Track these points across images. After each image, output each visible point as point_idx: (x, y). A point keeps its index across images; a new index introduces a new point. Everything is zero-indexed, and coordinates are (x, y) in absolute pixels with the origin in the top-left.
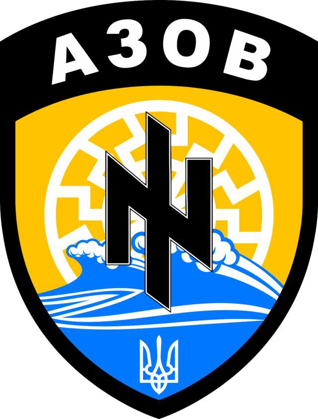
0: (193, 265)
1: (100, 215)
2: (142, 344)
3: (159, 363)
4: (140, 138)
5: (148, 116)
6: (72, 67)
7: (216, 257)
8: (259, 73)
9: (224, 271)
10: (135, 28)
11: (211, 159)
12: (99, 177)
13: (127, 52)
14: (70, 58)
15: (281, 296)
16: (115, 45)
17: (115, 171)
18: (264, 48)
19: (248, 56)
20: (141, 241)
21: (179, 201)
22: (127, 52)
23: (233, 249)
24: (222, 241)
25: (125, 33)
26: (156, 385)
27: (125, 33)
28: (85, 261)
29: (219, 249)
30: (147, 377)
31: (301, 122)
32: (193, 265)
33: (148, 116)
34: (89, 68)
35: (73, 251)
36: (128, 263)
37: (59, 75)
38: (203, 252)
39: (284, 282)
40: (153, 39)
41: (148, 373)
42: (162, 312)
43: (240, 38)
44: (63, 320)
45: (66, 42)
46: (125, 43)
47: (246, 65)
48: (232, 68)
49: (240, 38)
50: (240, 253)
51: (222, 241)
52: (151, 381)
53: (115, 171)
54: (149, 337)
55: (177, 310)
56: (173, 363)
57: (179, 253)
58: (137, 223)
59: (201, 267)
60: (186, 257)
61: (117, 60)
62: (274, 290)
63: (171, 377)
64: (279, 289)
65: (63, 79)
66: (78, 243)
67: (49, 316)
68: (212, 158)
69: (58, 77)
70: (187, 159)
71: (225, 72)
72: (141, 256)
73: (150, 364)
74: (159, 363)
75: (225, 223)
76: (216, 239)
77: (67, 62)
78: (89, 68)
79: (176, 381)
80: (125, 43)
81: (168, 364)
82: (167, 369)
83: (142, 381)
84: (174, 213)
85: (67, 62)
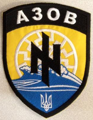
0: (55, 74)
1: (29, 59)
2: (42, 96)
3: (46, 101)
4: (41, 39)
6: (22, 20)
7: (62, 72)
8: (74, 22)
9: (64, 76)
10: (39, 10)
12: (29, 49)
13: (37, 16)
14: (22, 17)
15: (82, 84)
16: (34, 14)
17: (33, 47)
18: (75, 15)
19: (71, 18)
20: (41, 67)
21: (51, 55)
22: (37, 16)
23: (66, 70)
25: (37, 11)
26: (46, 109)
27: (37, 11)
28: (24, 71)
29: (63, 70)
30: (43, 106)
32: (55, 74)
34: (27, 20)
35: (22, 68)
37: (19, 22)
38: (58, 71)
39: (82, 80)
40: (44, 13)
41: (43, 104)
42: (47, 87)
43: (69, 13)
44: (19, 88)
45: (21, 13)
46: (36, 14)
47: (70, 20)
48: (66, 21)
49: (69, 13)
50: (69, 71)
52: (45, 107)
53: (33, 47)
54: (44, 94)
55: (50, 87)
56: (50, 102)
57: (51, 70)
58: (40, 62)
59: (57, 74)
60: (53, 72)
61: (35, 18)
62: (80, 83)
63: (50, 106)
64: (81, 82)
65: (20, 23)
66: (27, 66)
67: (14, 87)
69: (19, 22)
72: (40, 71)
73: (44, 102)
74: (46, 101)
75: (64, 63)
76: (62, 67)
78: (27, 20)
79: (51, 107)
80: (36, 14)
81: (49, 102)
82: (49, 104)
83: (41, 107)
84: (40, 59)
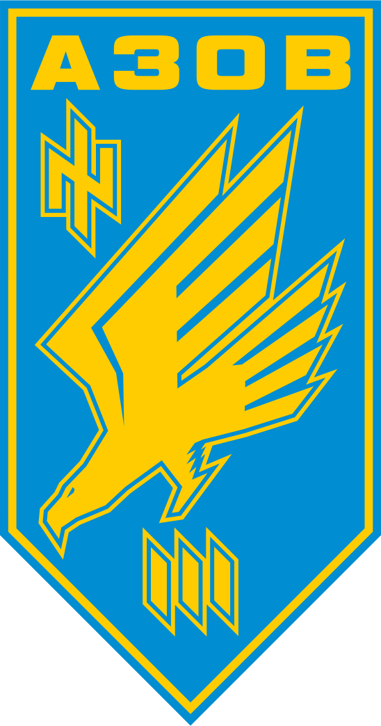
5: (97, 210)
6: (66, 76)
11: (161, 470)
14: (66, 64)
24: (162, 462)
31: (52, 89)
33: (97, 210)
36: (160, 474)
45: (65, 46)
51: (162, 462)
68: (161, 464)
70: (161, 470)
71: (9, 9)
77: (62, 67)
85: (62, 67)
